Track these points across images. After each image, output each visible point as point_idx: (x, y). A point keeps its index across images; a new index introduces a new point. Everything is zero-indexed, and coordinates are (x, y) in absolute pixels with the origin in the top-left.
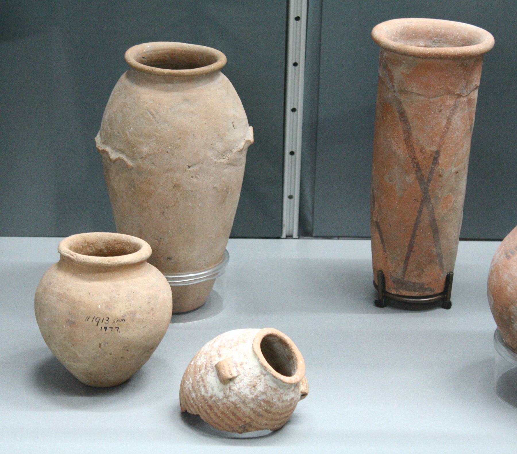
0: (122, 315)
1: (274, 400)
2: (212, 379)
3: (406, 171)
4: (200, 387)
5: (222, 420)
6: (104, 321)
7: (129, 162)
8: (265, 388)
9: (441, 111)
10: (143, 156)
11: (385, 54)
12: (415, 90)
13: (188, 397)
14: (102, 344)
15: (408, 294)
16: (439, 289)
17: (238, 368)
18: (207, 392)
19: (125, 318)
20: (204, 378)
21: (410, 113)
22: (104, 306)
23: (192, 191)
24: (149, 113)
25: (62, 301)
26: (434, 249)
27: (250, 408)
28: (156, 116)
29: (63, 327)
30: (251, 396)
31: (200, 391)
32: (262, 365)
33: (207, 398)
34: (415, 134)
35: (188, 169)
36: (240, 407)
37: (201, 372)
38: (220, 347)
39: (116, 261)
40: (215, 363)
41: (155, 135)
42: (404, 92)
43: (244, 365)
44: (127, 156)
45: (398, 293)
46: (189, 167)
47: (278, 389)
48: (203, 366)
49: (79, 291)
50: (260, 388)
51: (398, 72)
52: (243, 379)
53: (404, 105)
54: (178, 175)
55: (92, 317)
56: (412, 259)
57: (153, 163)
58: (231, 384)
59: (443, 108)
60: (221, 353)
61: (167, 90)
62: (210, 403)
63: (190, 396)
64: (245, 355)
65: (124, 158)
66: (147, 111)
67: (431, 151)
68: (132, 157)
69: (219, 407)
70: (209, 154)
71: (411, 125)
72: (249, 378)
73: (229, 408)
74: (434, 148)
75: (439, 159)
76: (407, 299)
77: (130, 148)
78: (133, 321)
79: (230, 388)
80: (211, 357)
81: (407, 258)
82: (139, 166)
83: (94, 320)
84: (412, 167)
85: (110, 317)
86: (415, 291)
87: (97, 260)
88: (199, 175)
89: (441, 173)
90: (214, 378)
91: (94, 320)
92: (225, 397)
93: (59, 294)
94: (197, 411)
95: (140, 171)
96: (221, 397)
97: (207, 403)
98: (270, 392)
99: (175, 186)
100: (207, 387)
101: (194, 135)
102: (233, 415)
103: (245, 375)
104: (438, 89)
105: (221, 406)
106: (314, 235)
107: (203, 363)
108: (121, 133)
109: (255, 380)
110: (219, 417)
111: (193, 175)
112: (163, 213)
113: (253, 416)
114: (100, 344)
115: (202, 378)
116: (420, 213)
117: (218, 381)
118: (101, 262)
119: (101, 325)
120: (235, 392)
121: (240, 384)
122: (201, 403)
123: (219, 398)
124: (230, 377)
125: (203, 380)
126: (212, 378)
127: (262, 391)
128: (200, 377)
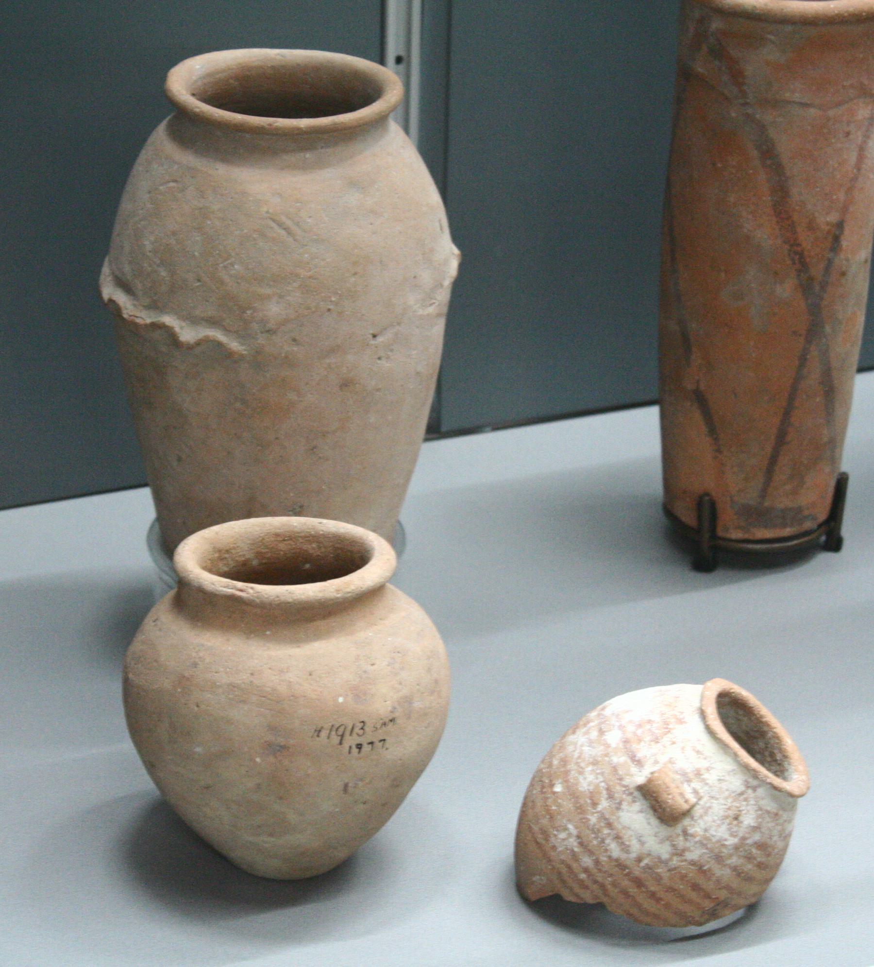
0: (390, 708)
1: (775, 838)
2: (635, 819)
3: (776, 273)
4: (603, 841)
5: (667, 906)
6: (357, 730)
7: (235, 345)
8: (758, 817)
9: (848, 134)
10: (270, 326)
11: (716, 24)
12: (797, 97)
13: (569, 867)
14: (350, 785)
15: (768, 534)
16: (822, 516)
17: (693, 785)
18: (625, 848)
19: (396, 714)
20: (613, 819)
21: (785, 146)
23: (378, 390)
25: (244, 702)
26: (825, 432)
27: (730, 867)
28: (294, 228)
29: (252, 760)
30: (732, 841)
31: (606, 850)
32: (746, 768)
33: (628, 863)
34: (798, 192)
35: (372, 342)
36: (710, 870)
37: (600, 808)
38: (626, 742)
39: (353, 587)
40: (640, 778)
42: (776, 104)
43: (706, 776)
44: (226, 330)
45: (746, 536)
46: (374, 336)
47: (781, 812)
49: (281, 671)
50: (749, 820)
51: (758, 63)
52: (710, 808)
53: (772, 133)
54: (350, 358)
55: (327, 726)
56: (784, 460)
57: (294, 340)
58: (686, 822)
59: (852, 128)
60: (639, 755)
61: (305, 167)
62: (637, 872)
63: (575, 865)
64: (698, 752)
65: (218, 335)
67: (828, 224)
68: (243, 335)
69: (661, 878)
70: (412, 299)
71: (788, 174)
72: (722, 802)
73: (686, 876)
74: (833, 217)
75: (842, 238)
76: (750, 546)
77: (235, 311)
79: (685, 833)
81: (773, 460)
82: (259, 352)
83: (333, 733)
84: (789, 262)
85: (366, 719)
86: (784, 526)
88: (392, 350)
89: (844, 269)
91: (333, 733)
92: (677, 854)
93: (233, 686)
96: (665, 856)
98: (768, 823)
99: (346, 384)
100: (626, 838)
101: (381, 262)
102: (694, 890)
103: (712, 797)
104: (844, 87)
106: (444, 429)
107: (597, 786)
109: (736, 804)
110: (658, 900)
112: (315, 447)
113: (735, 884)
114: (346, 786)
115: (606, 819)
116: (803, 359)
117: (654, 821)
118: (320, 595)
119: (351, 741)
120: (697, 839)
121: (706, 818)
122: (611, 875)
123: (659, 858)
124: (686, 807)
125: (609, 825)
126: (635, 817)
127: (752, 824)
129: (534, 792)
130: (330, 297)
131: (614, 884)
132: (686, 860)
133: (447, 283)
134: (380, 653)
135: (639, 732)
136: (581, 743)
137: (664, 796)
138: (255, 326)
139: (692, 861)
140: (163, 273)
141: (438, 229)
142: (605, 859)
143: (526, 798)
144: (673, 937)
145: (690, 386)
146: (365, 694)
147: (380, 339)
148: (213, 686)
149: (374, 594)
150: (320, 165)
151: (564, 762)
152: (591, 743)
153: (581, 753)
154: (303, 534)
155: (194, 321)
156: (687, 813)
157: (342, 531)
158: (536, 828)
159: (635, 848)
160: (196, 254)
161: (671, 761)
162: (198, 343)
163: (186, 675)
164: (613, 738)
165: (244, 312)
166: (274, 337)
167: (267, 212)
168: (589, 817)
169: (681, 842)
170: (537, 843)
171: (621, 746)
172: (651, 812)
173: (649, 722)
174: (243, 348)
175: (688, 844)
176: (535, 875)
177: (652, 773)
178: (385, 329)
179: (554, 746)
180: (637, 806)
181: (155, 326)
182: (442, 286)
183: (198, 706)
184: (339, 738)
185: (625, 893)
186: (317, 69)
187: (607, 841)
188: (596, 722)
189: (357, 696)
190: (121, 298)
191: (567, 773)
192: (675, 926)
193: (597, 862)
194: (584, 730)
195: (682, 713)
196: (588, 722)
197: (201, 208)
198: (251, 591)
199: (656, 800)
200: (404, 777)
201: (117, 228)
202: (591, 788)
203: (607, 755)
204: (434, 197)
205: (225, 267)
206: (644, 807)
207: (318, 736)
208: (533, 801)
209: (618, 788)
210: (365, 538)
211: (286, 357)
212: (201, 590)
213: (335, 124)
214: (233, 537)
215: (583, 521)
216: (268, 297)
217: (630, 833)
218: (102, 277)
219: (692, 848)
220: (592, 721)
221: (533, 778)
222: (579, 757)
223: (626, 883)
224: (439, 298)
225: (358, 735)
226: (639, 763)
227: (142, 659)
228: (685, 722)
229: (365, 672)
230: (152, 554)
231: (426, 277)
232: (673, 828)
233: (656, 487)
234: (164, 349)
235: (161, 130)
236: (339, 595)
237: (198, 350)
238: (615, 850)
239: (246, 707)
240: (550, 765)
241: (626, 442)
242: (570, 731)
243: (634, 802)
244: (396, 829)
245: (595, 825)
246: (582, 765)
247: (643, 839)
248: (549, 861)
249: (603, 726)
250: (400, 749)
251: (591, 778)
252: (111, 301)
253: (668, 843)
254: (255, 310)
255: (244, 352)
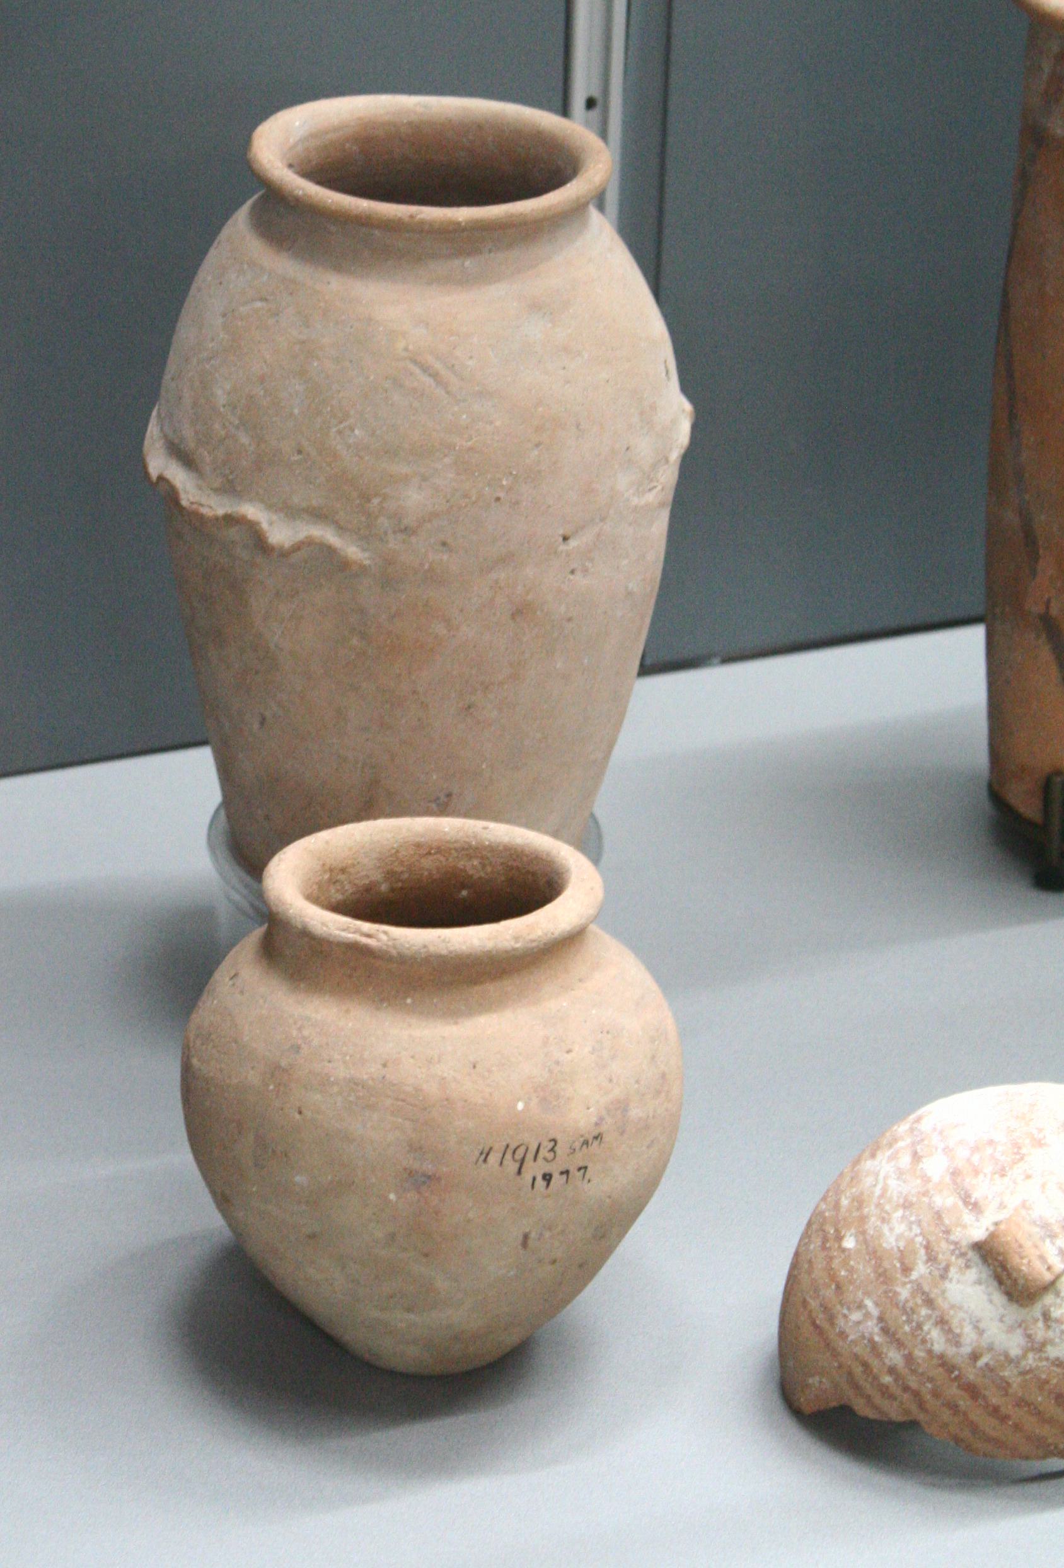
0: (594, 1119)
2: (970, 1295)
4: (919, 1326)
5: (1017, 1427)
6: (543, 1152)
7: (353, 551)
10: (408, 521)
13: (865, 1365)
14: (533, 1235)
18: (955, 1339)
19: (604, 1128)
22: (535, 1101)
23: (570, 620)
24: (417, 371)
25: (372, 1107)
31: (924, 1341)
33: (958, 1361)
35: (562, 547)
37: (914, 1275)
38: (955, 1173)
39: (540, 933)
40: (978, 1233)
41: (451, 447)
44: (341, 529)
46: (565, 539)
48: (914, 1252)
49: (430, 1061)
54: (529, 572)
55: (499, 1147)
57: (444, 544)
58: (1049, 1299)
60: (976, 1195)
61: (465, 281)
62: (971, 1375)
63: (874, 1363)
65: (328, 535)
66: (411, 367)
68: (366, 535)
70: (623, 481)
77: (354, 499)
78: (622, 1133)
79: (1046, 1316)
80: (938, 1216)
85: (559, 1138)
87: (476, 942)
88: (592, 560)
90: (979, 1289)
91: (508, 1156)
92: (1032, 1349)
93: (354, 1083)
94: (914, 1408)
95: (389, 576)
96: (1015, 1352)
97: (957, 1378)
99: (521, 611)
100: (955, 1323)
101: (578, 426)
105: (1016, 1382)
108: (314, 453)
110: (1004, 1419)
111: (575, 566)
114: (526, 1237)
115: (923, 1293)
117: (999, 1298)
118: (490, 945)
119: (534, 1169)
123: (1006, 1355)
124: (1048, 1277)
125: (929, 1302)
126: (970, 1290)
128: (913, 1294)
129: (812, 1247)
130: (500, 480)
131: (936, 1394)
132: (1047, 1359)
133: (675, 455)
134: (575, 1033)
135: (975, 1159)
136: (885, 1174)
137: (1015, 1260)
138: (384, 522)
139: (1057, 1359)
140: (244, 439)
141: (664, 374)
142: (922, 1354)
143: (797, 1254)
144: (1025, 1474)
145: (1034, 608)
146: (558, 1097)
147: (573, 543)
148: (325, 1083)
149: (568, 943)
150: (483, 278)
151: (859, 1202)
152: (900, 1173)
153: (884, 1190)
154: (457, 845)
155: (291, 512)
156: (1049, 1287)
157: (519, 841)
158: (813, 1304)
159: (969, 1337)
160: (296, 411)
161: (1024, 1205)
162: (297, 547)
163: (283, 1063)
164: (936, 1167)
165: (369, 501)
166: (414, 539)
167: (406, 349)
168: (898, 1289)
169: (1040, 1331)
170: (816, 1327)
171: (947, 1179)
172: (995, 1284)
173: (991, 1142)
174: (366, 555)
175: (1050, 1334)
176: (813, 1376)
177: (996, 1224)
178: (583, 527)
179: (841, 1175)
180: (972, 1274)
181: (230, 520)
182: (667, 461)
183: (300, 1113)
184: (517, 1165)
185: (954, 1408)
186: (479, 127)
187: (926, 1328)
188: (908, 1141)
189: (543, 1100)
190: (179, 477)
191: (863, 1219)
192: (1027, 1458)
193: (909, 1358)
194: (888, 1153)
195: (1040, 1130)
196: (896, 1140)
197: (304, 342)
198: (384, 937)
199: (1004, 1267)
200: (611, 1225)
201: (171, 368)
202: (902, 1244)
203: (925, 1193)
204: (655, 326)
205: (340, 432)
206: (984, 1276)
207: (485, 1160)
208: (810, 1262)
209: (944, 1245)
210: (554, 852)
211: (431, 569)
212: (305, 934)
213: (512, 215)
214: (350, 849)
215: (857, 806)
216: (406, 479)
217: (961, 1315)
218: (147, 442)
219: (1057, 1340)
220: (902, 1139)
221: (809, 1224)
222: (882, 1196)
223: (953, 1391)
224: (663, 479)
225: (545, 1159)
226: (976, 1207)
227: (213, 1037)
228: (1045, 1144)
229: (557, 1063)
230: (215, 859)
231: (644, 447)
232: (1027, 1309)
233: (978, 756)
234: (245, 555)
235: (242, 216)
236: (518, 945)
237: (295, 558)
238: (938, 1341)
239: (375, 1116)
240: (837, 1206)
241: (929, 684)
242: (867, 1154)
243: (967, 1267)
244: (600, 1301)
245: (907, 1301)
246: (887, 1207)
247: (981, 1325)
248: (835, 1354)
249: (919, 1148)
250: (605, 1183)
251: (900, 1228)
252: (161, 478)
253: (1019, 1331)
254: (385, 497)
255: (367, 562)
